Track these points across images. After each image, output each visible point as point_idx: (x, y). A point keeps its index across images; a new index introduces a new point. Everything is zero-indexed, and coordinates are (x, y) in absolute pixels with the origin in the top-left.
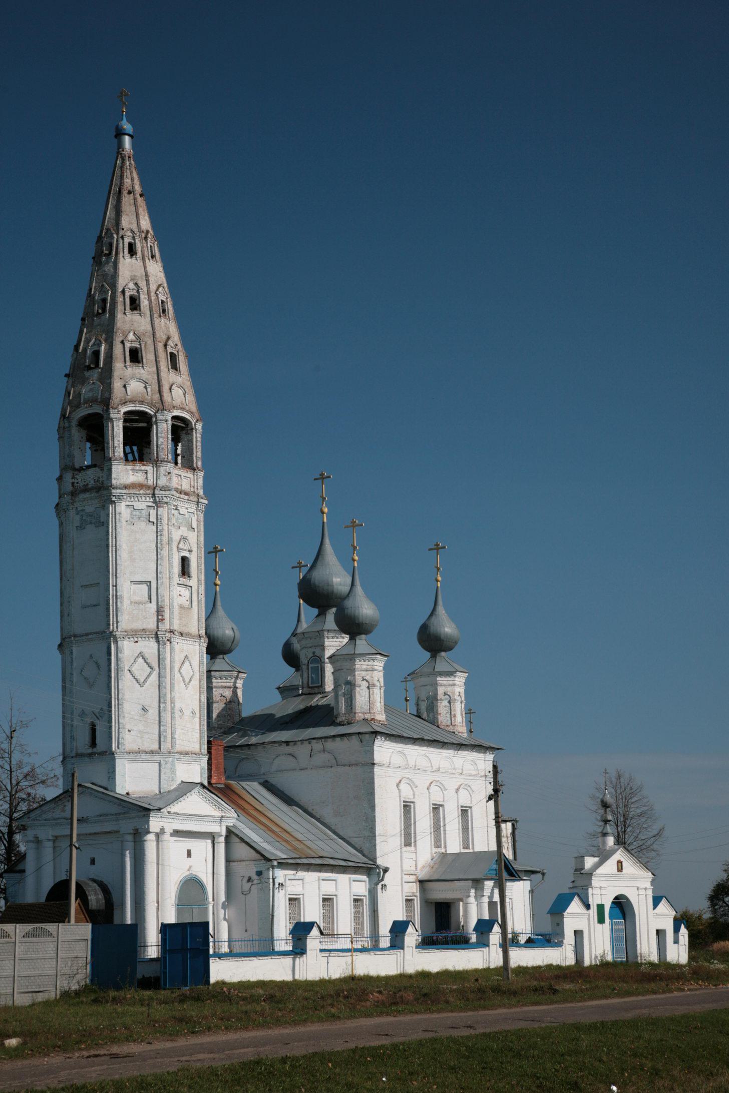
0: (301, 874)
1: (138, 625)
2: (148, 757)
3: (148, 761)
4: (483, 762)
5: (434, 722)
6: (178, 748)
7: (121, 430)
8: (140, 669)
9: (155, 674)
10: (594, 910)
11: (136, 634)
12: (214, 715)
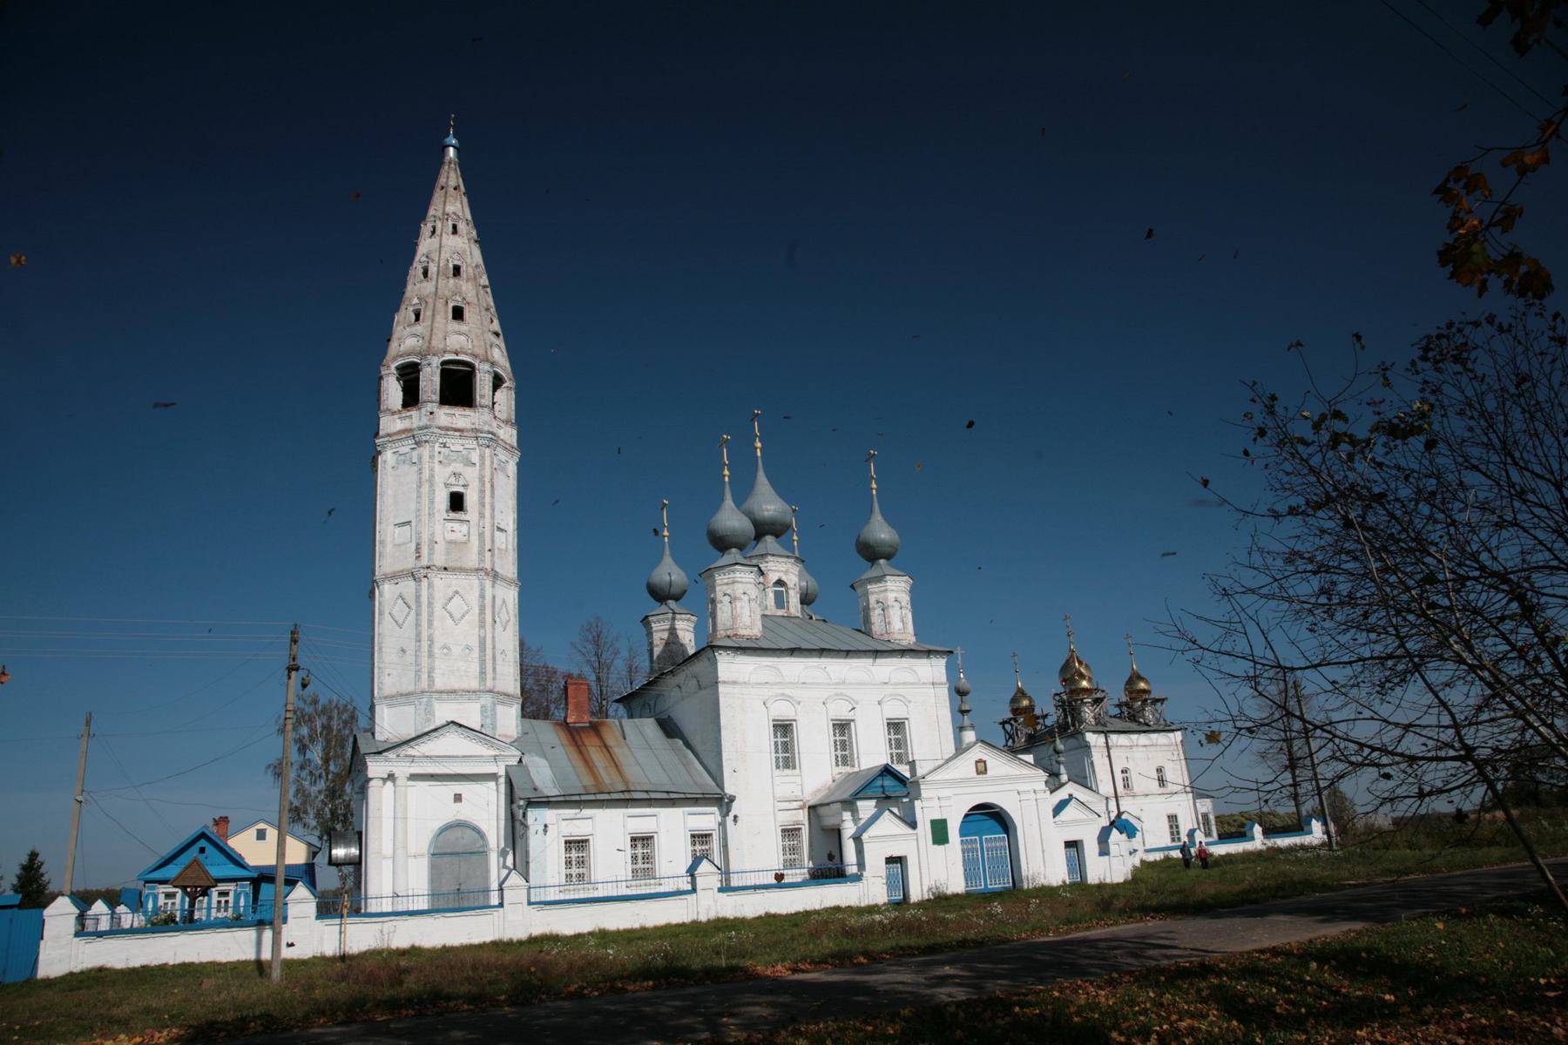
0: (587, 812)
1: (398, 567)
2: (403, 700)
3: (404, 704)
4: (934, 669)
5: (868, 633)
6: (439, 684)
7: (437, 379)
8: (399, 610)
9: (413, 613)
10: (924, 829)
11: (394, 577)
12: (657, 651)
